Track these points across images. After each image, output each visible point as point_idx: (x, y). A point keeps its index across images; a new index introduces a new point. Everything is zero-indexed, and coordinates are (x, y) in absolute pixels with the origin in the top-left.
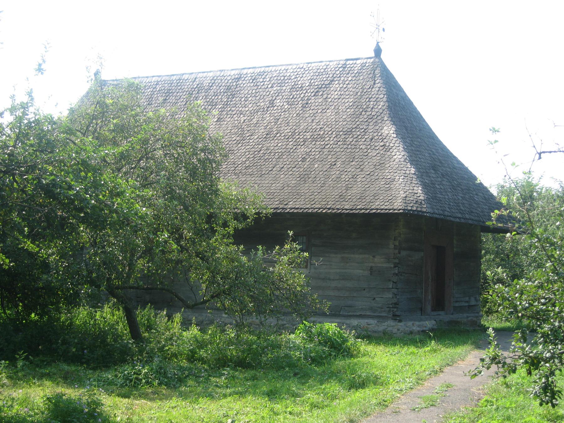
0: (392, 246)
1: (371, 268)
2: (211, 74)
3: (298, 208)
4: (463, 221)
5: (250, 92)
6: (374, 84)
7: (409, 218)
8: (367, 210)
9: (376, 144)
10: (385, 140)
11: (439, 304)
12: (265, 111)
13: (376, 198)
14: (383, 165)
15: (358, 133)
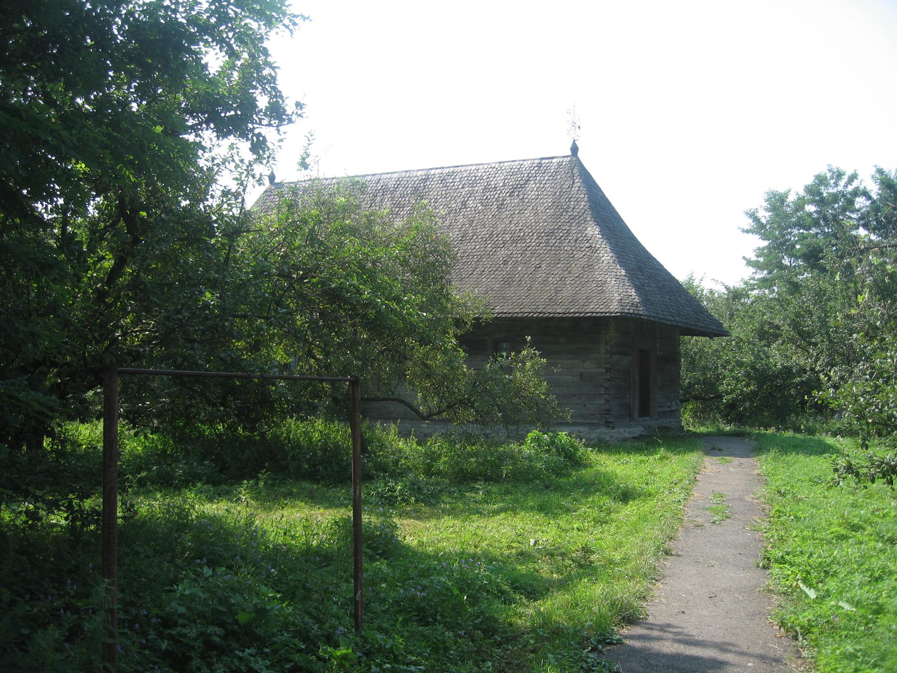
1: (581, 374)
2: (396, 175)
4: (674, 323)
7: (624, 324)
9: (582, 245)
11: (645, 411)
12: (457, 212)
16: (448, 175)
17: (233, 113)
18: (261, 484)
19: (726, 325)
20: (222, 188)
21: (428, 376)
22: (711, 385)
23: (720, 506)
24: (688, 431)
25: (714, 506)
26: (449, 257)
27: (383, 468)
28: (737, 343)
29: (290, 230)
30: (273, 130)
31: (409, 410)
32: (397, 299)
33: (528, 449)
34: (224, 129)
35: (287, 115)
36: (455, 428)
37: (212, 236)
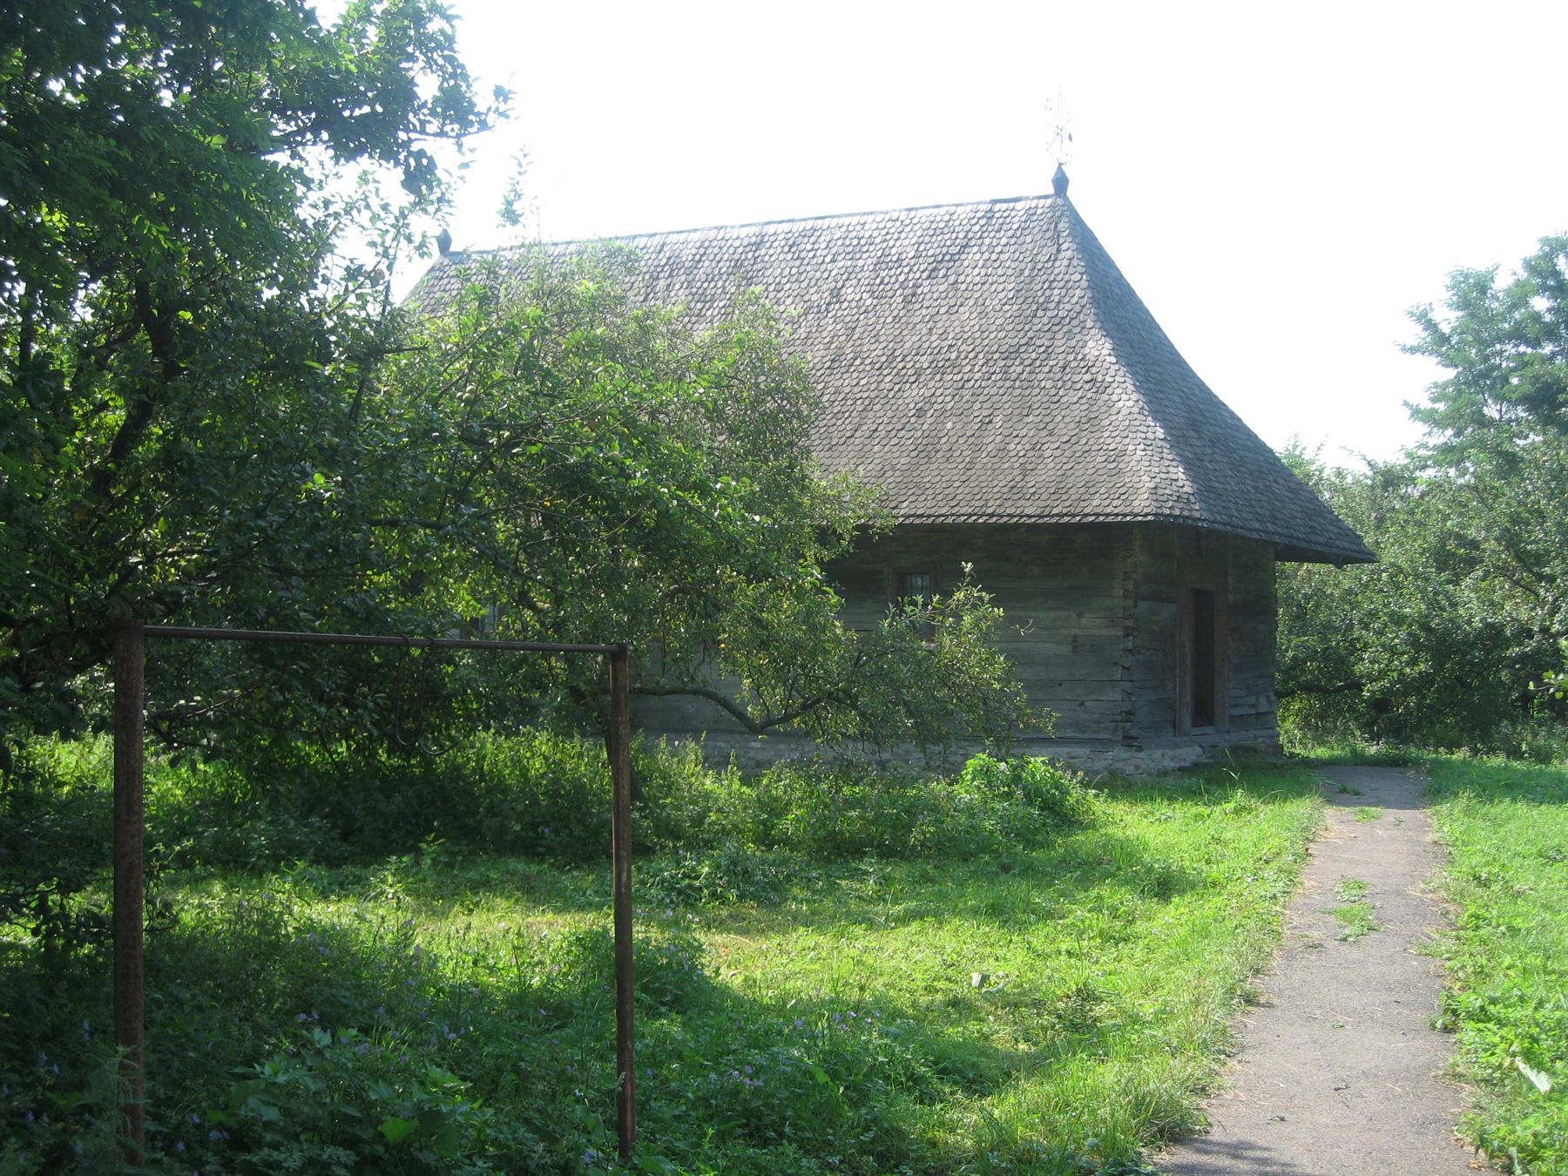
1: (1075, 639)
2: (697, 236)
3: (921, 516)
5: (786, 272)
6: (1058, 251)
7: (1161, 536)
8: (1074, 516)
10: (1094, 370)
11: (1204, 714)
13: (1092, 491)
14: (1095, 422)
15: (1034, 356)
16: (803, 234)
17: (366, 109)
19: (1368, 540)
21: (764, 645)
23: (1356, 906)
25: (1345, 907)
28: (1391, 576)
29: (483, 348)
30: (447, 144)
31: (725, 712)
32: (703, 489)
33: (966, 791)
34: (351, 140)
35: (478, 114)
37: (326, 359)
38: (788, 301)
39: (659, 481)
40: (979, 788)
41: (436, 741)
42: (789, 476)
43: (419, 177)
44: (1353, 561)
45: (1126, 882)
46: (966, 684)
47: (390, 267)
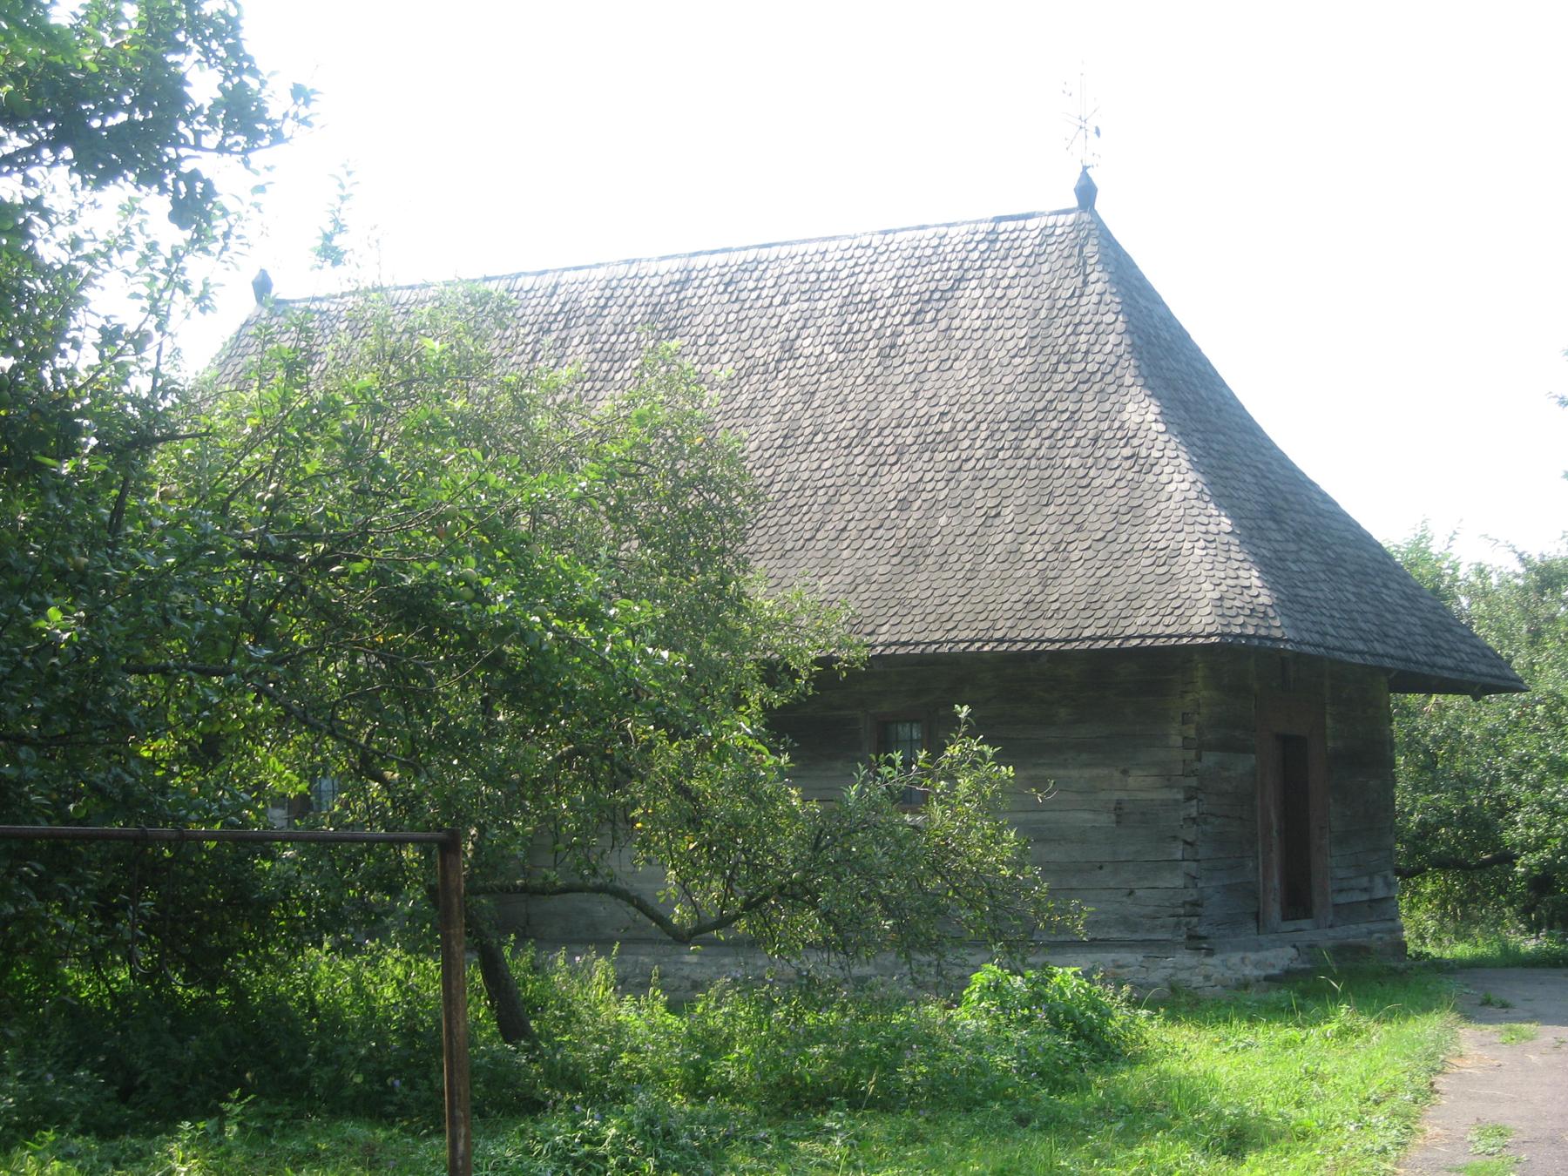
0: (1179, 741)
1: (1119, 805)
2: (600, 273)
3: (906, 644)
4: (1370, 660)
5: (721, 320)
6: (1085, 283)
7: (1231, 663)
8: (1112, 639)
10: (1136, 442)
11: (1298, 902)
12: (771, 370)
13: (1136, 604)
14: (1139, 511)
15: (1055, 424)
17: (122, 117)
18: (232, 1130)
19: (1519, 664)
20: (101, 322)
21: (694, 822)
22: (1482, 827)
23: (1495, 1161)
24: (1419, 956)
25: (1479, 1162)
26: (741, 491)
27: (570, 1079)
28: (1549, 709)
29: (290, 431)
30: (231, 161)
31: (640, 916)
32: (592, 616)
33: (971, 1017)
34: (99, 159)
35: (270, 122)
36: (768, 962)
37: (68, 449)
38: (725, 358)
39: (531, 607)
40: (988, 1011)
41: (250, 962)
42: (720, 596)
43: (193, 207)
44: (1498, 690)
45: (1186, 1134)
46: (964, 871)
47: (159, 327)
